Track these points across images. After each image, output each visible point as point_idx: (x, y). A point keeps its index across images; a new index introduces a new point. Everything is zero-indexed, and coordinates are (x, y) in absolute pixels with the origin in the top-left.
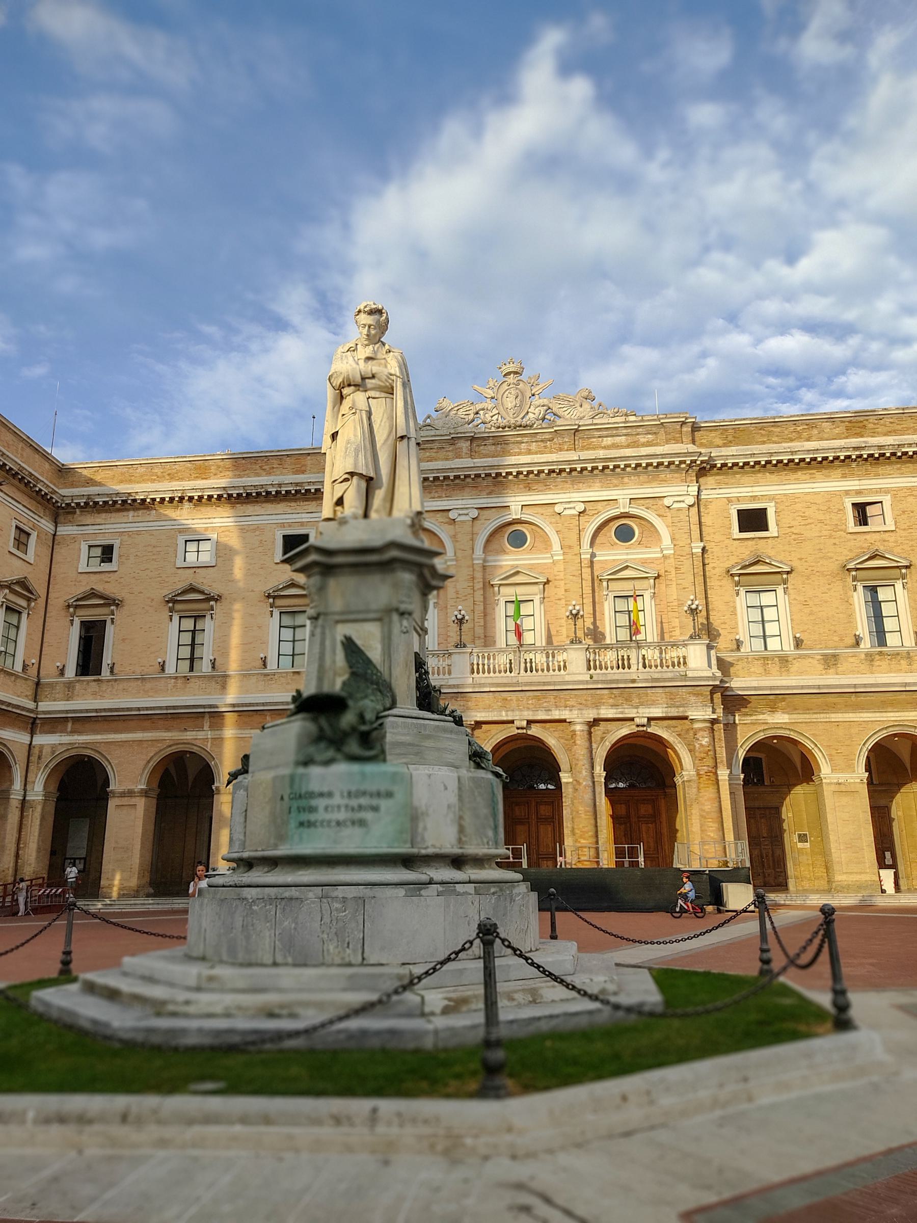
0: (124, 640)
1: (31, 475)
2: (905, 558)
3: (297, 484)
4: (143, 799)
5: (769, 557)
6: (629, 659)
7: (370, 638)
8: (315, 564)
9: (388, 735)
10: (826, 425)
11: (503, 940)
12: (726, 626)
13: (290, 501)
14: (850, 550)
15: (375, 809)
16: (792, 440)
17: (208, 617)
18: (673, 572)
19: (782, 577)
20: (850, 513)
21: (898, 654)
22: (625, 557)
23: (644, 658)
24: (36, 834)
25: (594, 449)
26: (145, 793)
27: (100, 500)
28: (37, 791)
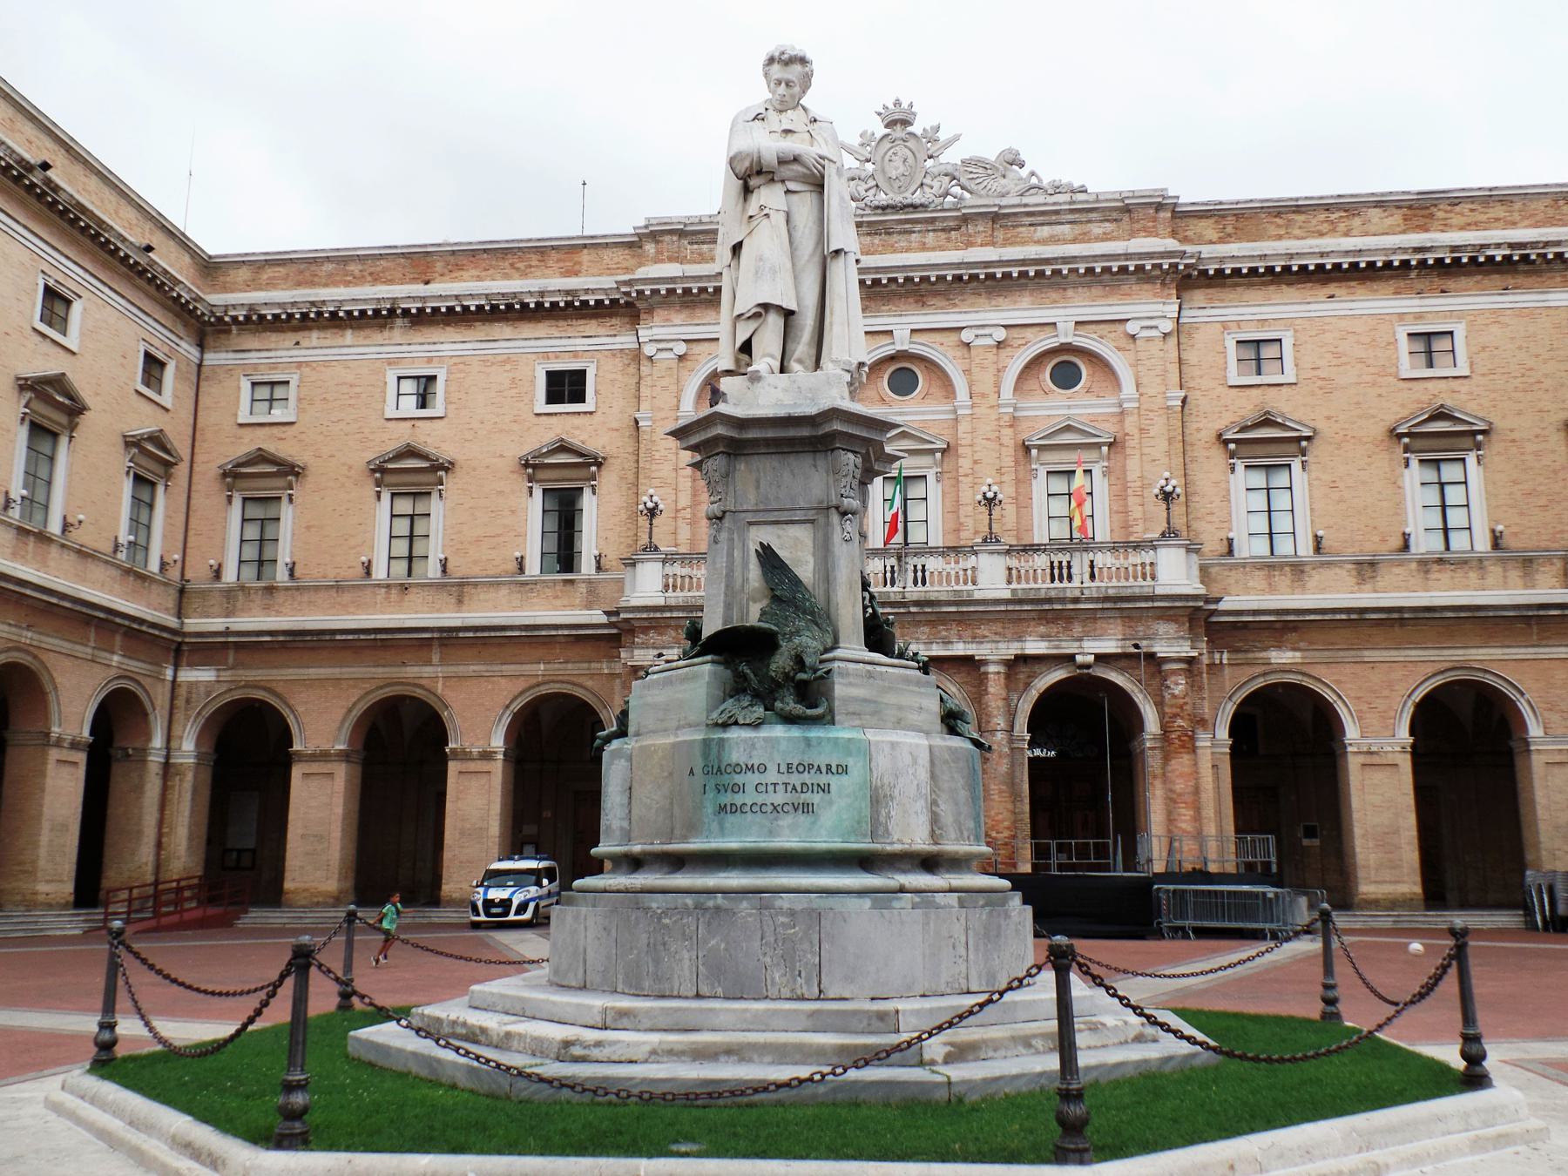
0: (308, 528)
1: (166, 272)
2: (1482, 419)
3: (568, 293)
4: (344, 765)
5: (1282, 415)
6: (1069, 567)
7: (796, 547)
8: (716, 440)
9: (837, 687)
10: (1374, 213)
12: (1214, 518)
13: (557, 318)
14: (1403, 406)
15: (825, 789)
16: (1322, 235)
17: (435, 495)
18: (1137, 436)
22: (1066, 412)
23: (1092, 566)
24: (187, 813)
25: (1023, 243)
26: (345, 756)
27: (268, 313)
28: (187, 747)
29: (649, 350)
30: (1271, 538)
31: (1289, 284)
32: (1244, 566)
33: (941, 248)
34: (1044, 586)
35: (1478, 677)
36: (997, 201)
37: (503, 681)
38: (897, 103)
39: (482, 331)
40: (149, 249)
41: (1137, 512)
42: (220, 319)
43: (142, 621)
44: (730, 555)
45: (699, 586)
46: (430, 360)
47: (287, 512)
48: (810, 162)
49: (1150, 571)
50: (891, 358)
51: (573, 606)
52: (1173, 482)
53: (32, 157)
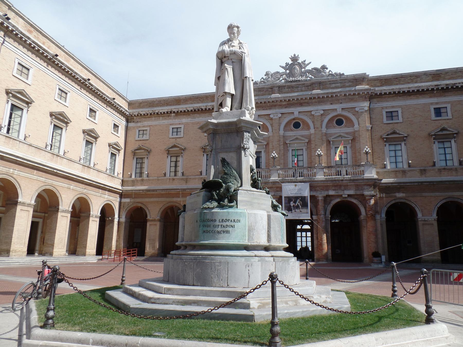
2: (456, 130)
6: (340, 172)
11: (280, 282)
16: (409, 83)
19: (404, 139)
20: (433, 112)
21: (452, 169)
23: (347, 171)
31: (400, 96)
33: (306, 91)
35: (456, 200)
38: (295, 55)
40: (114, 99)
47: (146, 161)
50: (294, 119)
53: (86, 78)
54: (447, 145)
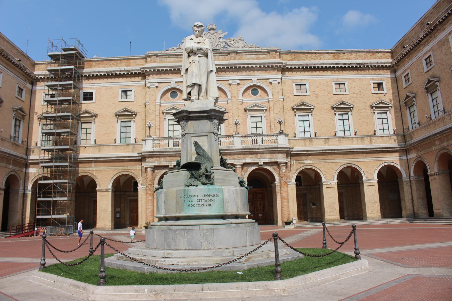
1: (24, 66)
3: (127, 71)
6: (257, 140)
7: (204, 143)
15: (213, 200)
23: (262, 140)
25: (243, 59)
29: (148, 85)
30: (302, 133)
32: (299, 139)
34: (251, 146)
36: (237, 49)
37: (111, 171)
39: (105, 80)
41: (273, 126)
42: (37, 78)
43: (17, 157)
44: (187, 144)
45: (162, 146)
46: (91, 88)
48: (205, 50)
49: (276, 141)
51: (129, 152)
52: (282, 119)
54: (345, 117)
